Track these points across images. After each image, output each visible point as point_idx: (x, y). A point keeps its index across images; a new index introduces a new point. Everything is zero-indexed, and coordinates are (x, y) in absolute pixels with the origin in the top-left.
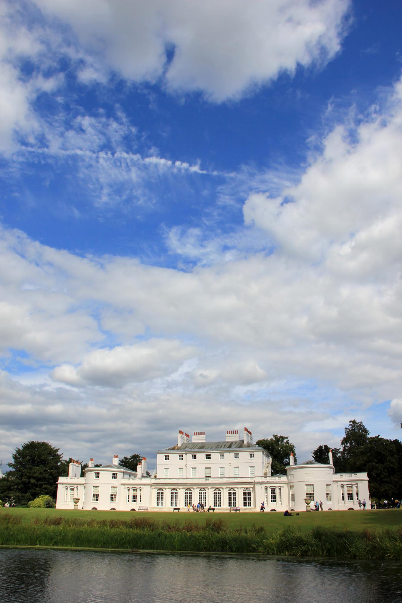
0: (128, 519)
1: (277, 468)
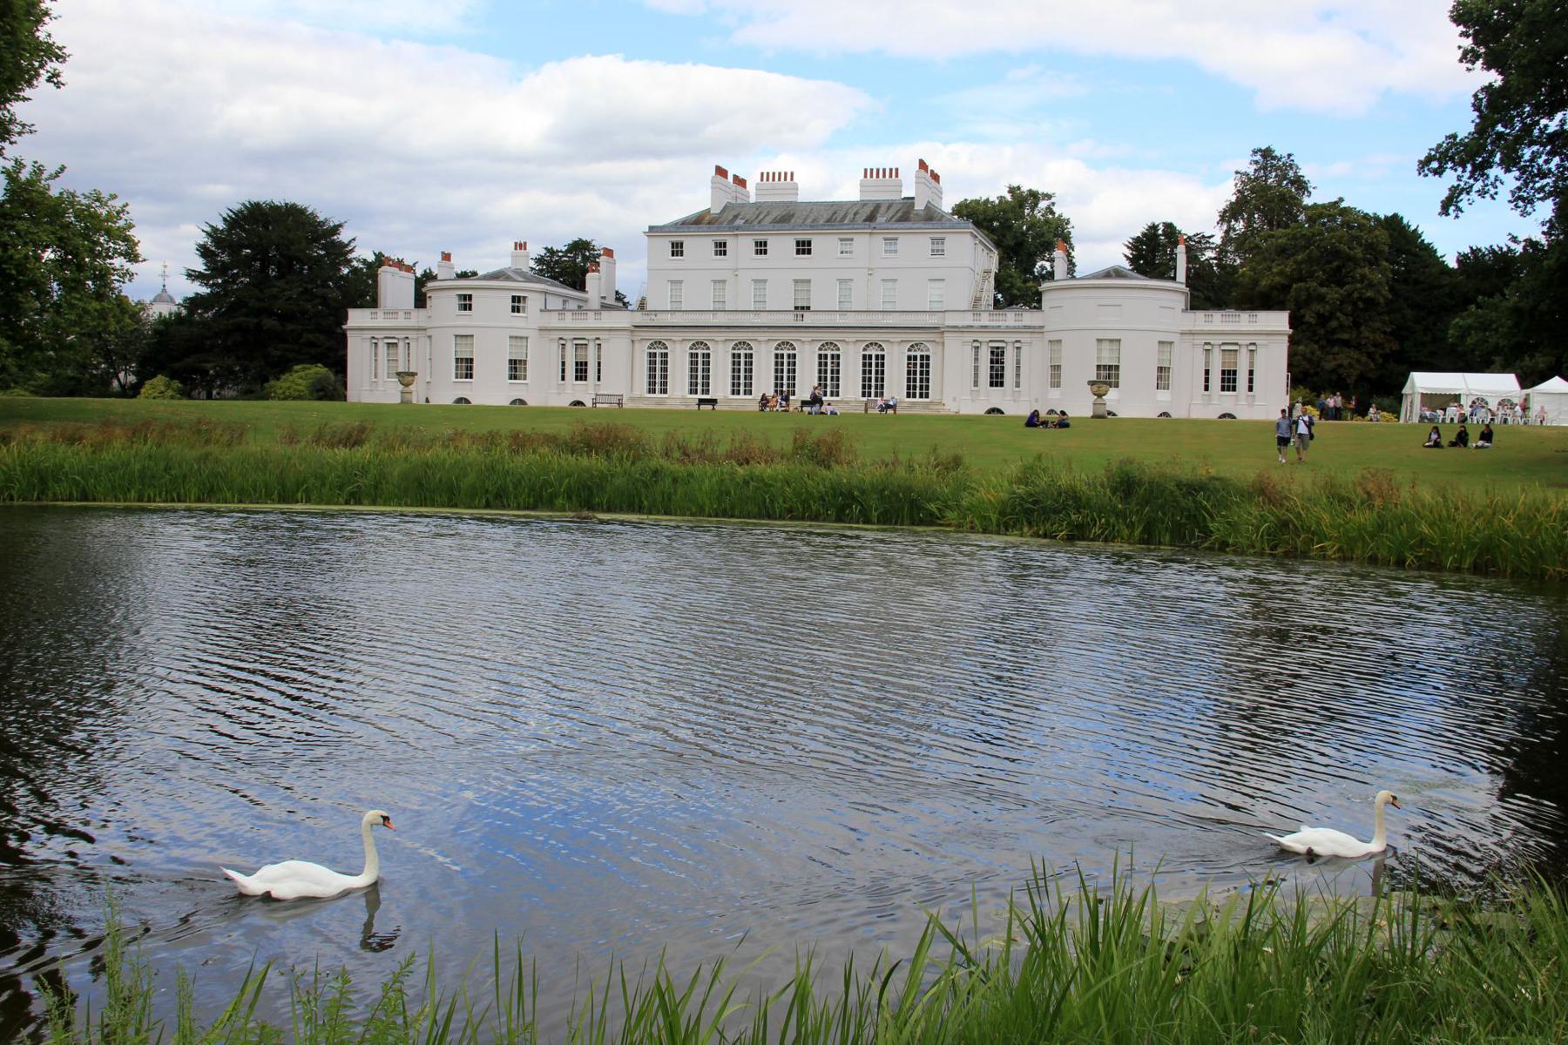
0: (564, 430)
1: (1012, 286)
